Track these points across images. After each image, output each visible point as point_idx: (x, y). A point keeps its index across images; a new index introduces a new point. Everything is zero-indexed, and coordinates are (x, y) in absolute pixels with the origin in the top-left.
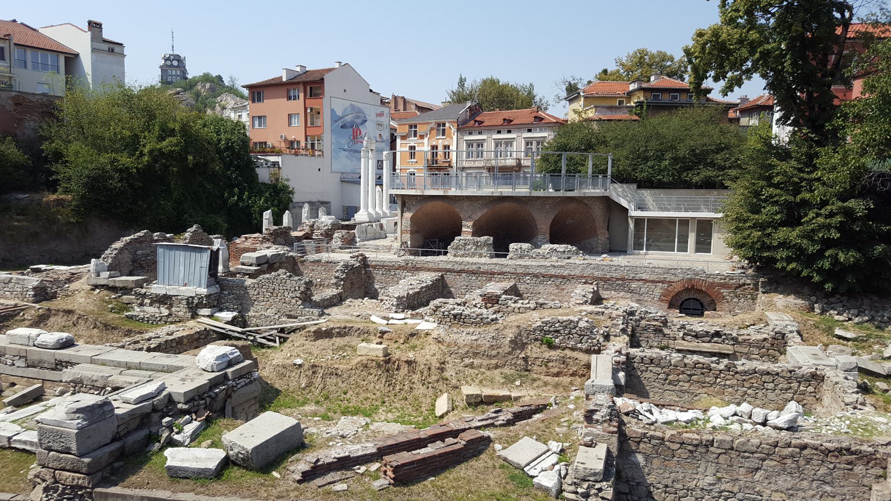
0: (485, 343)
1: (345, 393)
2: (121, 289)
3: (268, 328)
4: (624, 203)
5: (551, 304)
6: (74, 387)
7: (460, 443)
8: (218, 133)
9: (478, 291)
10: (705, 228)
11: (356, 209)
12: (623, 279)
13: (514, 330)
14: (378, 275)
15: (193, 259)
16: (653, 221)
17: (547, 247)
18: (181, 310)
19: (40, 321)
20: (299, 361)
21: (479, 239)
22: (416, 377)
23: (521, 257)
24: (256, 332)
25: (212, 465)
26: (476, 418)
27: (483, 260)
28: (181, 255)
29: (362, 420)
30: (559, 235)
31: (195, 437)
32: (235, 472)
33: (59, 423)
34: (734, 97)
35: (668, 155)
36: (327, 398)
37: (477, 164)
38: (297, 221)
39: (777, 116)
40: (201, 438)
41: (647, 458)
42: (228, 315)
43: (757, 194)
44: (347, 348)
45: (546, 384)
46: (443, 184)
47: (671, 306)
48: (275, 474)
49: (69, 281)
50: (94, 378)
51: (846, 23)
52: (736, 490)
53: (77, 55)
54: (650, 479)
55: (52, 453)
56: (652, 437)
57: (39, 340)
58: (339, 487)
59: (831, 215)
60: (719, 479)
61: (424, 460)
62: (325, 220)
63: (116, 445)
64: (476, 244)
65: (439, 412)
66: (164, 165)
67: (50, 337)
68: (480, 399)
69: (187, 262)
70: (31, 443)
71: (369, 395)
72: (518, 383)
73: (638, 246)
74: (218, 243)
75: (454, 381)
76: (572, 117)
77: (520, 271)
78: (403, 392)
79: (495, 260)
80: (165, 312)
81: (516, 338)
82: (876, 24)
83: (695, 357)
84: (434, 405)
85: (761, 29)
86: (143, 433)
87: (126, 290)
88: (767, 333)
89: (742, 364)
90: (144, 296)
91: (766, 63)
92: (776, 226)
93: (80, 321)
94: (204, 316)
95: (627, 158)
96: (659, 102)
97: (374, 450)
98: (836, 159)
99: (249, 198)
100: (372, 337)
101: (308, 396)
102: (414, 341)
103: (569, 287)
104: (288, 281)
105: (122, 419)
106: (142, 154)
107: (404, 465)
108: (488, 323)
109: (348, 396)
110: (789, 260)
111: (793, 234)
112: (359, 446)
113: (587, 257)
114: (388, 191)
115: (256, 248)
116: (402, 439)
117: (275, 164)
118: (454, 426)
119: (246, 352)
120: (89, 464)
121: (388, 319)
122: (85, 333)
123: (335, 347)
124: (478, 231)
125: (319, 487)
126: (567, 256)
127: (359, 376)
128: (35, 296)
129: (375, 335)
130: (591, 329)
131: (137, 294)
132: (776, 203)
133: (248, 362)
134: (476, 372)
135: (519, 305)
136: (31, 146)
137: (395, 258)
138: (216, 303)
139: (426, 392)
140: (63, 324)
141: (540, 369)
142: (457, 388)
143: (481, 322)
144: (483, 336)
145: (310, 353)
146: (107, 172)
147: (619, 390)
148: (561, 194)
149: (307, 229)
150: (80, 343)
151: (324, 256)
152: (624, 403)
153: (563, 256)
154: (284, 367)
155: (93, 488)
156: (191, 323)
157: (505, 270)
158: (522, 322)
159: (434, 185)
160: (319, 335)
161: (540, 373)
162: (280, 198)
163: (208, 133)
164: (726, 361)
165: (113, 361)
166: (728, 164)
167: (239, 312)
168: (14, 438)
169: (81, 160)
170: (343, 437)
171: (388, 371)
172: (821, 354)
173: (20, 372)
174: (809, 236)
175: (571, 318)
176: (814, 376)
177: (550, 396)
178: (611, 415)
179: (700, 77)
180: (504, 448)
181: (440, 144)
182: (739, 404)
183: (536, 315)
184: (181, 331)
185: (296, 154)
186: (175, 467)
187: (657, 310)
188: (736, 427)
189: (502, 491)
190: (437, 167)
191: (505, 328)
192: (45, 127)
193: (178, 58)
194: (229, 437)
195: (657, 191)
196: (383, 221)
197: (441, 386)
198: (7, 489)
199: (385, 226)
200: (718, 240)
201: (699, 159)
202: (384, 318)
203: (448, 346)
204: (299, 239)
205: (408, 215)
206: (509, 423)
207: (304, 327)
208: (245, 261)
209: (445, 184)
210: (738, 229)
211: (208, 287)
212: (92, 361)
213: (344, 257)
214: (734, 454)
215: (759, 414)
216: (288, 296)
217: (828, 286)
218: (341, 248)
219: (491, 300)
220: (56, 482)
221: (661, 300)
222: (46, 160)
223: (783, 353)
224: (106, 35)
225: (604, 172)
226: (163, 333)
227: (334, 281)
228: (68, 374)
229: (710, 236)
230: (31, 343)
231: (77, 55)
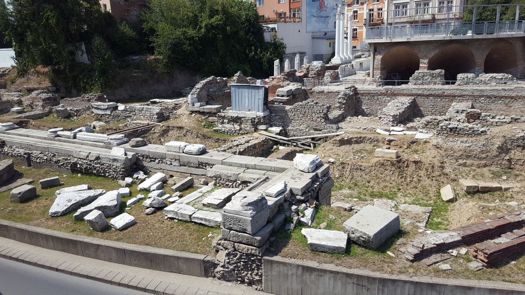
1: (369, 182)
2: (207, 113)
6: (216, 180)
13: (501, 139)
15: (253, 94)
18: (248, 126)
20: (332, 160)
21: (434, 72)
22: (422, 173)
23: (467, 83)
24: (297, 140)
27: (437, 87)
30: (490, 67)
31: (313, 218)
32: (356, 250)
33: (237, 213)
36: (356, 185)
37: (402, 20)
42: (277, 129)
44: (362, 151)
50: (229, 175)
55: (232, 232)
57: (187, 149)
66: (214, 34)
67: (195, 147)
68: (477, 189)
69: (250, 96)
71: (387, 184)
75: (453, 176)
77: (476, 93)
78: (413, 183)
79: (447, 87)
80: (238, 128)
81: (503, 145)
84: (439, 193)
87: (211, 114)
90: (224, 117)
93: (188, 133)
94: (262, 130)
97: (459, 238)
99: (261, 52)
100: (381, 144)
101: (342, 183)
102: (414, 147)
104: (315, 107)
105: (271, 208)
106: (201, 28)
107: (494, 253)
108: (479, 134)
109: (371, 184)
113: (520, 82)
117: (273, 29)
120: (260, 241)
121: (389, 131)
123: (354, 151)
124: (432, 66)
125: (429, 266)
126: (503, 81)
127: (378, 171)
128: (158, 118)
129: (383, 142)
134: (469, 169)
135: (496, 120)
138: (269, 121)
139: (431, 183)
140: (178, 135)
142: (455, 180)
145: (338, 155)
146: (181, 40)
153: (501, 82)
155: (262, 257)
156: (256, 135)
157: (464, 93)
158: (507, 133)
161: (521, 170)
162: (278, 50)
165: (237, 163)
167: (283, 127)
168: (194, 215)
169: (166, 33)
171: (399, 168)
173: (175, 169)
181: (375, 8)
186: (316, 244)
191: (493, 137)
192: (143, 14)
197: (443, 179)
198: (199, 251)
199: (355, 66)
202: (386, 130)
203: (445, 151)
205: (379, 57)
208: (280, 94)
209: (380, 36)
211: (264, 111)
212: (223, 163)
213: (341, 88)
216: (315, 116)
218: (330, 82)
227: (338, 105)
228: (211, 172)
230: (181, 151)
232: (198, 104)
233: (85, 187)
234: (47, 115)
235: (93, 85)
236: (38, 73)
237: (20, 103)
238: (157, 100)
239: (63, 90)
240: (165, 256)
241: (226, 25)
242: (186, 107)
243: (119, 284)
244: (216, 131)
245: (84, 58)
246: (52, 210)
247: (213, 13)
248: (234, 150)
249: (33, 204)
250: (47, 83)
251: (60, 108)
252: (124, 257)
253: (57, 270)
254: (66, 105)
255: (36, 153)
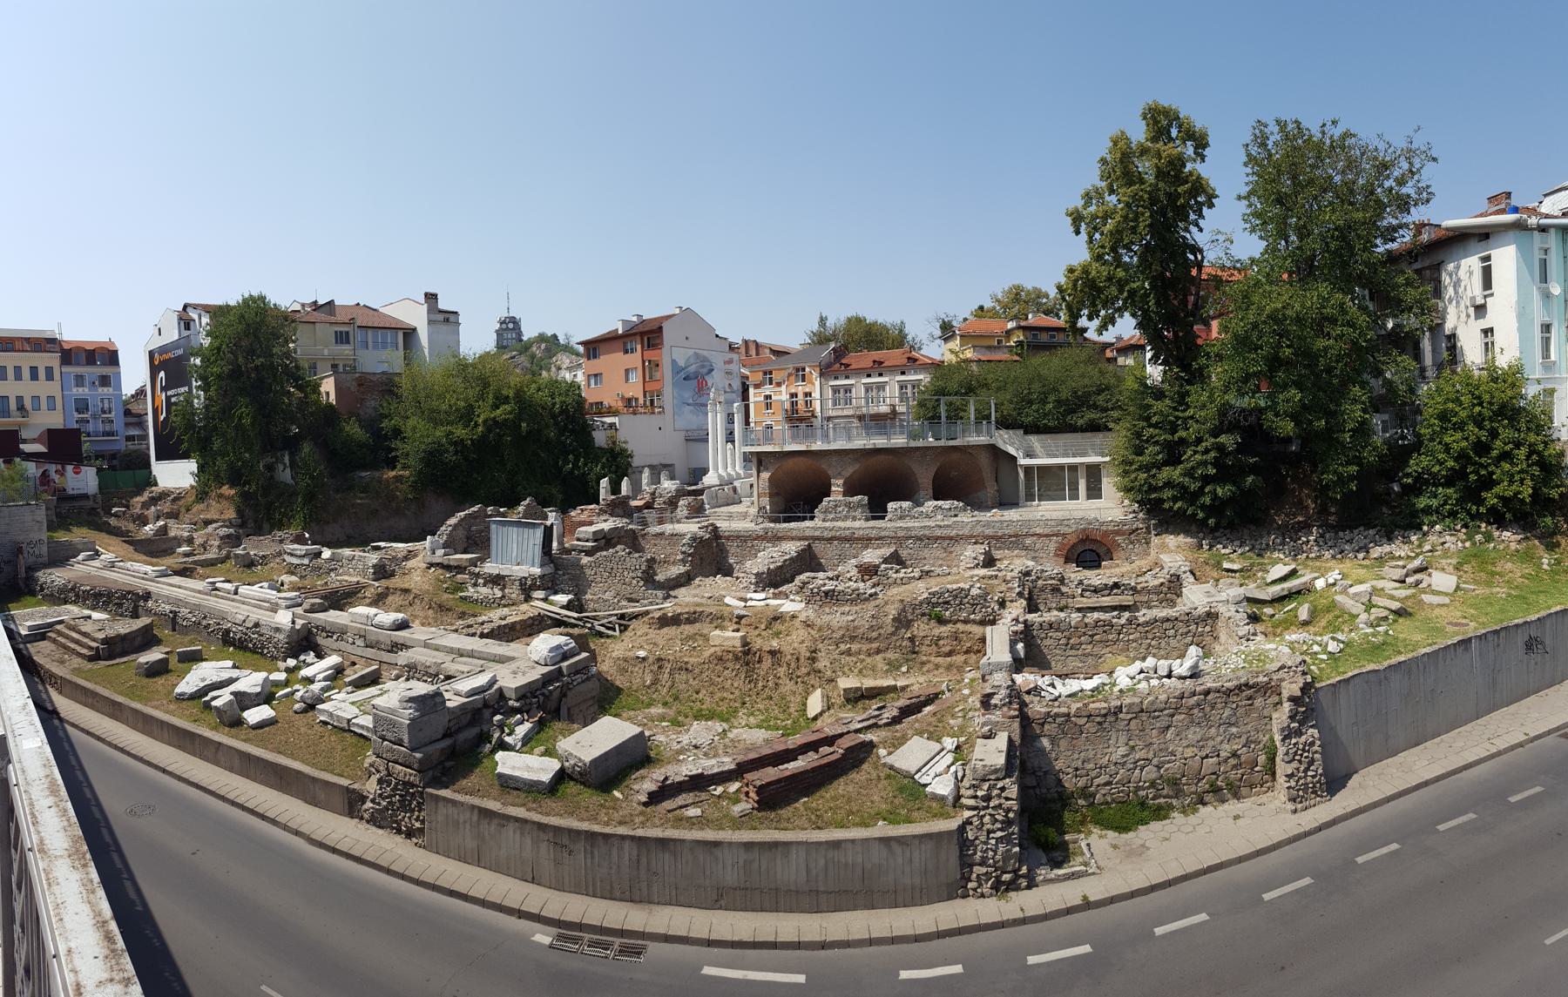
0: (863, 624)
3: (607, 614)
4: (1012, 451)
5: (938, 570)
7: (838, 751)
8: (552, 396)
9: (853, 561)
10: (1094, 473)
11: (705, 471)
12: (1016, 536)
14: (732, 548)
16: (1043, 469)
17: (931, 504)
18: (514, 592)
19: (378, 601)
20: (642, 654)
22: (782, 671)
24: (594, 618)
25: (546, 777)
26: (855, 718)
27: (857, 524)
28: (514, 532)
29: (719, 726)
30: (941, 491)
31: (527, 740)
33: (392, 712)
34: (1109, 336)
35: (1052, 398)
38: (636, 489)
39: (1149, 355)
40: (533, 743)
41: (1053, 741)
43: (1138, 435)
45: (937, 666)
46: (806, 437)
47: (1067, 560)
48: (617, 794)
49: (406, 558)
51: (1200, 265)
52: (1150, 756)
53: (415, 330)
54: (1059, 765)
56: (1057, 715)
57: (377, 620)
58: (693, 812)
59: (1207, 451)
60: (1133, 748)
61: (794, 777)
62: (668, 485)
63: (447, 742)
64: (848, 505)
65: (811, 713)
67: (388, 617)
70: (368, 729)
72: (904, 669)
73: (1030, 497)
74: (552, 517)
76: (949, 358)
77: (901, 534)
79: (872, 523)
80: (499, 594)
82: (1223, 268)
83: (1096, 615)
84: (805, 705)
85: (1126, 267)
86: (474, 731)
87: (460, 569)
88: (1163, 577)
89: (1144, 615)
90: (478, 575)
91: (1134, 302)
92: (1159, 466)
95: (1011, 402)
96: (1038, 341)
98: (1205, 397)
100: (727, 623)
102: (778, 626)
103: (957, 549)
106: (476, 425)
108: (866, 600)
110: (1175, 499)
111: (1174, 473)
112: (713, 761)
114: (740, 448)
115: (594, 522)
116: (766, 751)
117: (612, 425)
118: (829, 732)
119: (582, 643)
120: (420, 760)
121: (745, 600)
122: (421, 614)
124: (849, 491)
130: (984, 596)
131: (471, 574)
132: (1156, 443)
133: (584, 655)
136: (371, 425)
137: (751, 526)
138: (550, 585)
141: (929, 650)
143: (858, 598)
144: (860, 616)
147: (1018, 665)
148: (942, 443)
149: (648, 497)
150: (416, 625)
151: (668, 528)
152: (1024, 679)
154: (625, 660)
156: (524, 607)
159: (794, 438)
160: (665, 621)
162: (618, 463)
163: (543, 397)
164: (1127, 614)
166: (1110, 405)
169: (419, 434)
170: (696, 747)
172: (1213, 590)
174: (1189, 474)
175: (962, 585)
176: (1209, 614)
177: (942, 681)
178: (1010, 696)
179: (1074, 316)
180: (890, 754)
182: (1144, 659)
183: (921, 585)
184: (515, 615)
185: (634, 413)
187: (1053, 567)
188: (1143, 685)
189: (889, 807)
190: (798, 418)
193: (514, 320)
194: (565, 744)
195: (1043, 436)
196: (737, 484)
197: (813, 680)
200: (1108, 484)
201: (1081, 401)
204: (639, 509)
205: (765, 475)
206: (896, 721)
207: (647, 613)
210: (1126, 472)
212: (426, 645)
213: (691, 528)
214: (1144, 716)
215: (1163, 666)
216: (628, 576)
217: (1211, 521)
219: (868, 571)
220: (389, 775)
221: (1056, 555)
222: (386, 437)
223: (1179, 595)
224: (442, 306)
225: (988, 417)
226: (495, 616)
227: (680, 557)
228: (403, 658)
229: (1100, 481)
231: (415, 330)
232: (440, 552)
233: (229, 663)
234: (223, 561)
235: (293, 517)
236: (221, 496)
237: (190, 541)
238: (382, 544)
239: (251, 524)
240: (299, 772)
241: (522, 420)
242: (420, 560)
243: (233, 803)
244: (464, 599)
245: (285, 475)
246: (178, 690)
247: (501, 400)
248: (472, 630)
249: (160, 681)
250: (231, 514)
251: (239, 551)
252: (249, 767)
253: (164, 771)
254: (252, 547)
255: (184, 611)
